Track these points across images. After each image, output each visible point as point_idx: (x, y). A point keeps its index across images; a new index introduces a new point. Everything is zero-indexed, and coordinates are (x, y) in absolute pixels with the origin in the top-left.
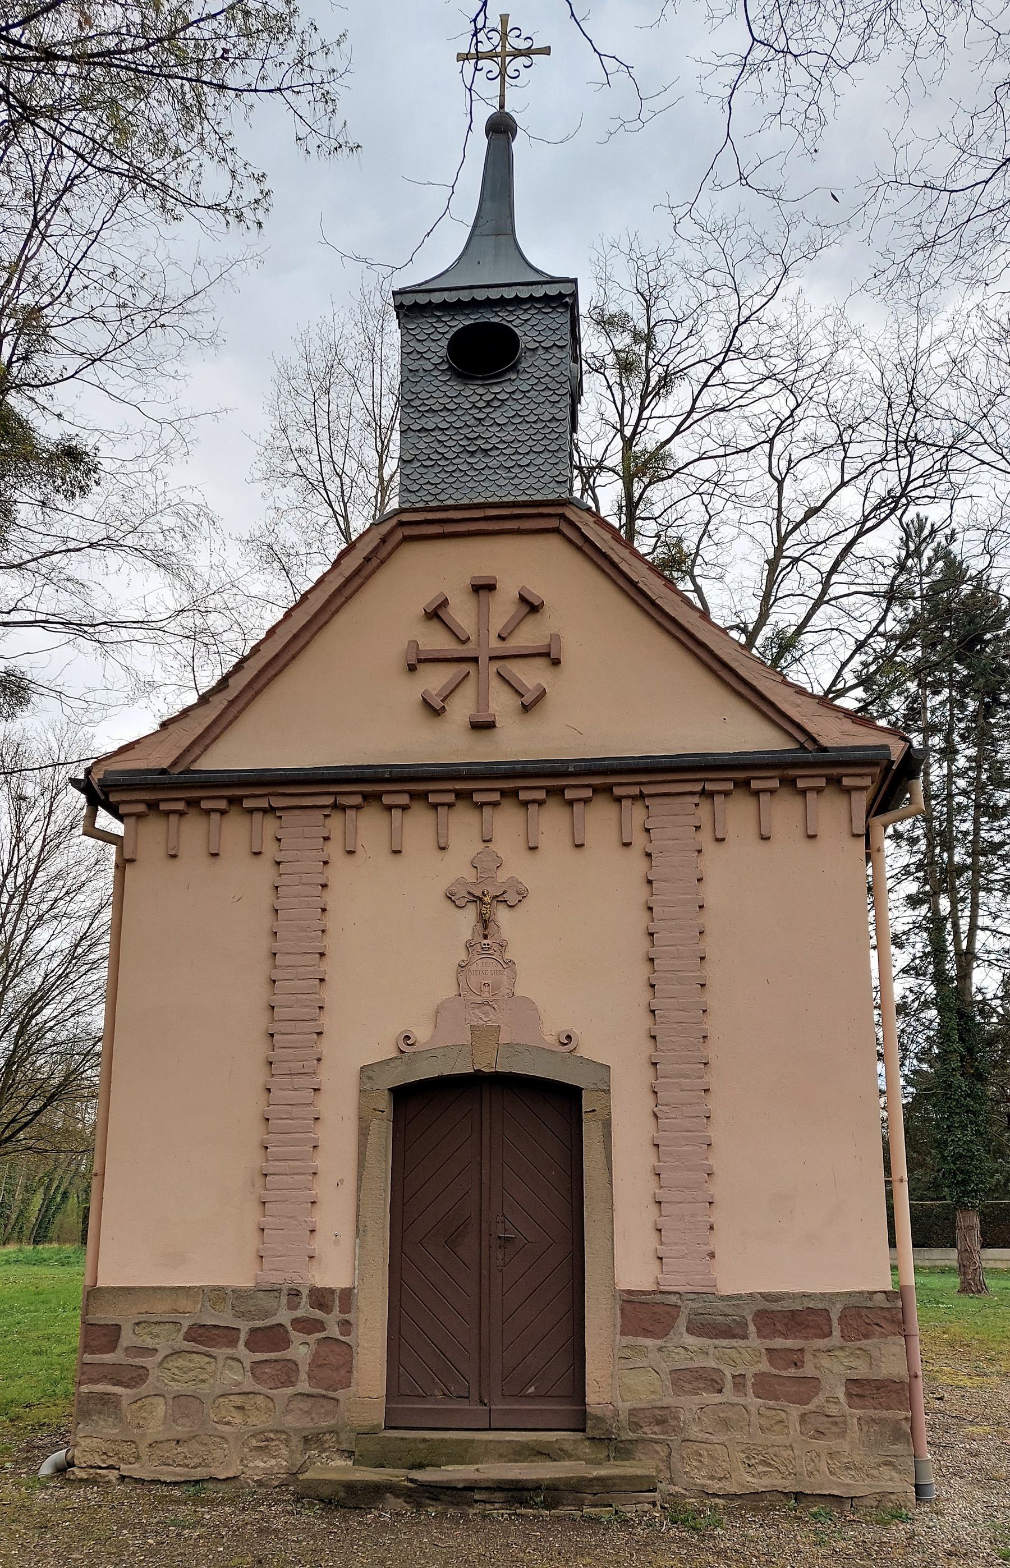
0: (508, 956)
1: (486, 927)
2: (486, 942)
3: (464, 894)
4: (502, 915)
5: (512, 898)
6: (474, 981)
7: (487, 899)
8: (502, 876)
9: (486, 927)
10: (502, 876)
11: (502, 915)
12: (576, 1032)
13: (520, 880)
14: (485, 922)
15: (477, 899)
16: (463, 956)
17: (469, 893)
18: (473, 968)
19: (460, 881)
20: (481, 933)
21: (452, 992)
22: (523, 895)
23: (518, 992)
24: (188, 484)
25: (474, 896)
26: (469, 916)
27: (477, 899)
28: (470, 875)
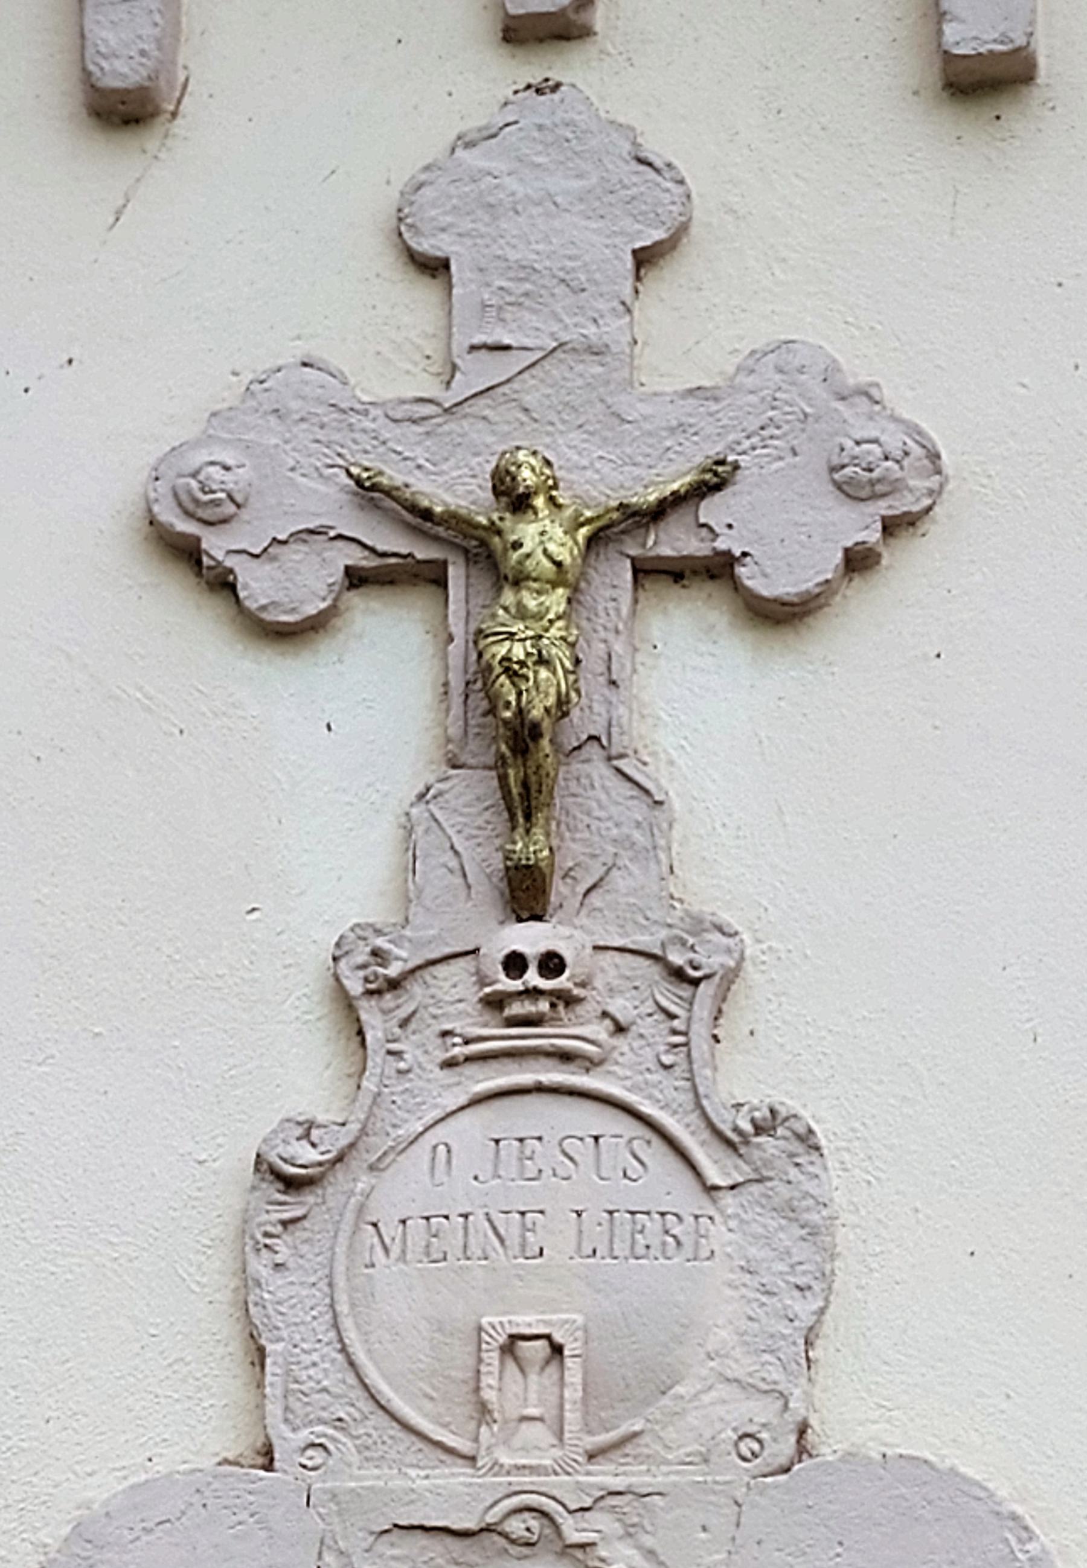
0: (741, 1082)
1: (524, 800)
2: (530, 938)
3: (326, 501)
4: (682, 692)
5: (781, 532)
6: (409, 1317)
7: (543, 538)
8: (687, 342)
9: (524, 800)
10: (687, 342)
11: (682, 692)
12: (107, 484)
13: (856, 374)
14: (517, 751)
15: (434, 554)
16: (298, 1081)
17: (369, 492)
18: (402, 1190)
19: (287, 395)
20: (484, 859)
21: (192, 1423)
22: (891, 515)
23: (859, 1410)
24: (654, 1208)
25: (420, 517)
26: (387, 678)
27: (434, 554)
28: (381, 343)
